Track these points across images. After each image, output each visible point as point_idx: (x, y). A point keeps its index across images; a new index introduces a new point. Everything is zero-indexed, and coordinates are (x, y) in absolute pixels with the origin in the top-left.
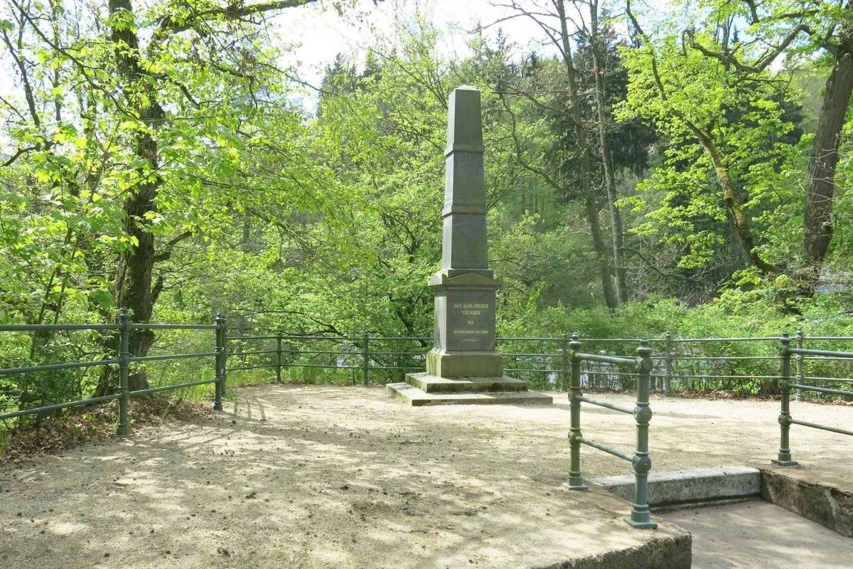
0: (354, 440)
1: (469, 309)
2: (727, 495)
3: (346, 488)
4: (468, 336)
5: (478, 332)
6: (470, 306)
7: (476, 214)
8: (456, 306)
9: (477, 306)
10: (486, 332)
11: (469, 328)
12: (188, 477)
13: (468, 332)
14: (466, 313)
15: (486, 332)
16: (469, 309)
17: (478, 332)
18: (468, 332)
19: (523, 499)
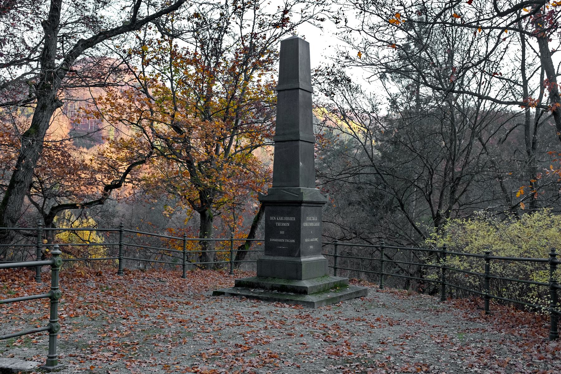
4: (281, 244)
5: (287, 241)
6: (281, 219)
9: (287, 219)
10: (294, 241)
11: (281, 237)
13: (280, 240)
17: (287, 241)
18: (280, 240)
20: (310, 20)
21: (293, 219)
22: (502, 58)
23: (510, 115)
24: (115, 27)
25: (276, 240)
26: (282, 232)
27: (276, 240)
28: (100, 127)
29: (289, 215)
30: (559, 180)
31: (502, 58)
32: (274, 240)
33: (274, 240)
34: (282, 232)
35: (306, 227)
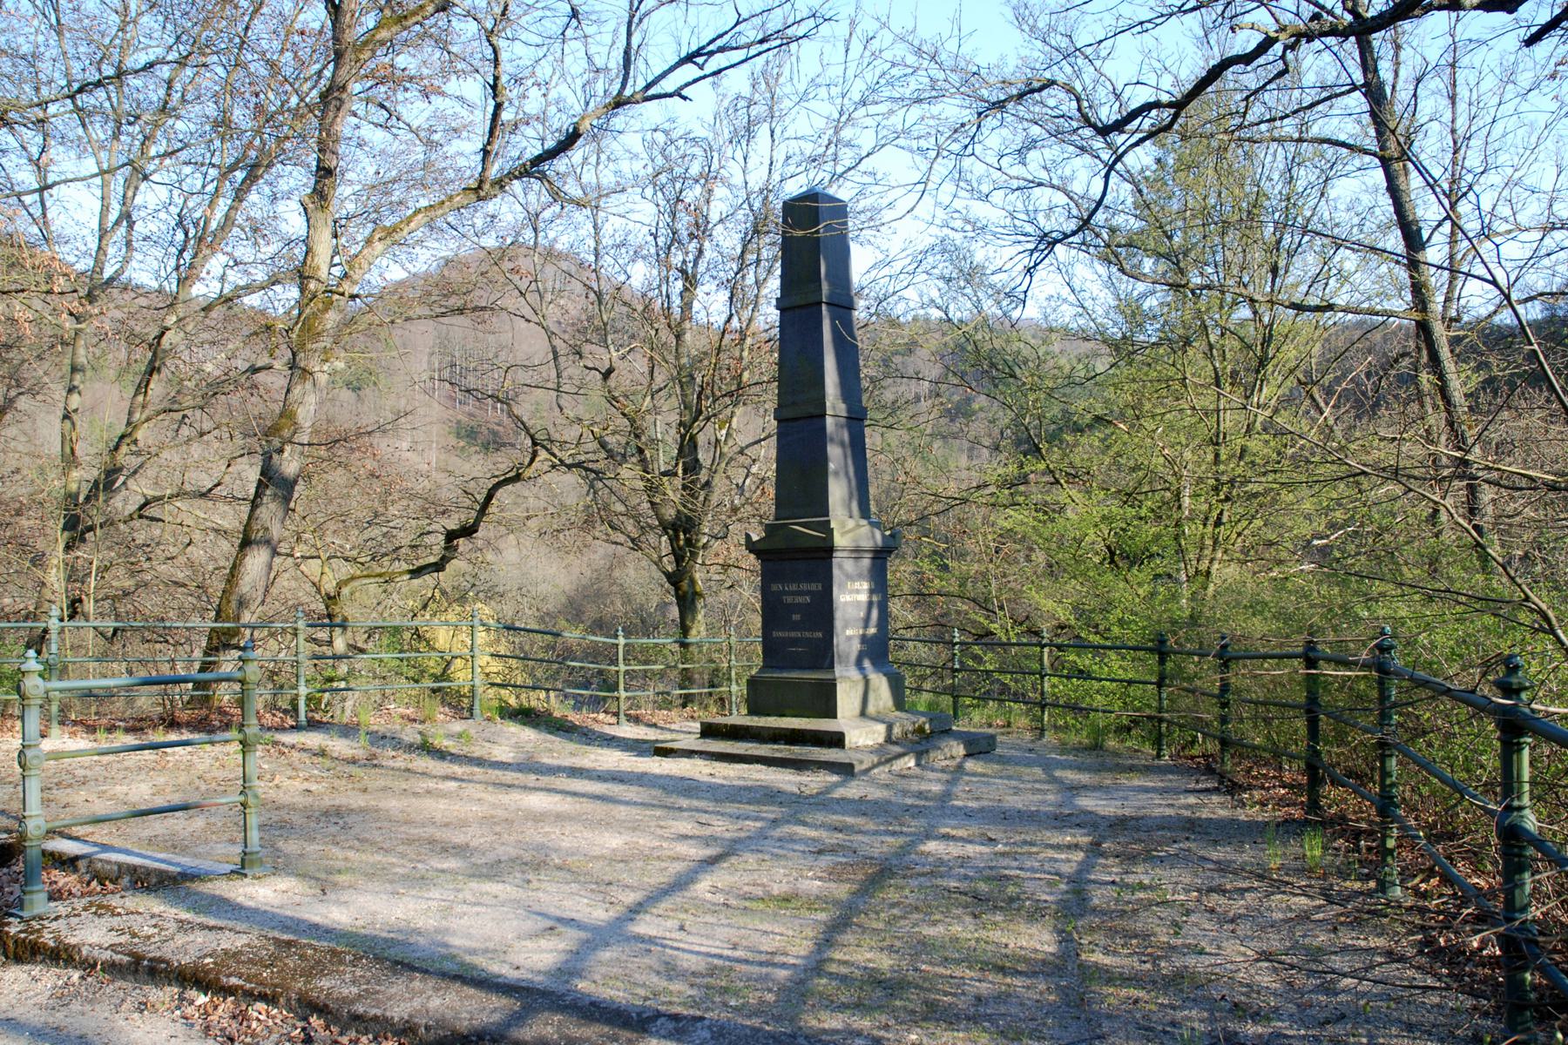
0: (611, 741)
1: (793, 593)
2: (759, 767)
3: (365, 790)
4: (794, 642)
5: (808, 634)
6: (794, 587)
7: (811, 417)
8: (775, 587)
9: (804, 587)
10: (820, 635)
11: (795, 626)
12: (1365, 831)
13: (793, 634)
14: (789, 599)
15: (820, 635)
16: (793, 593)
17: (808, 634)
18: (793, 634)
19: (1432, 185)
20: (901, 142)
21: (816, 587)
22: (247, 28)
23: (826, 861)
24: (861, 363)
25: (786, 634)
26: (796, 617)
27: (786, 634)
28: (24, 668)
29: (809, 578)
30: (316, 17)
31: (247, 28)
32: (780, 634)
33: (780, 634)
34: (796, 617)
35: (846, 603)
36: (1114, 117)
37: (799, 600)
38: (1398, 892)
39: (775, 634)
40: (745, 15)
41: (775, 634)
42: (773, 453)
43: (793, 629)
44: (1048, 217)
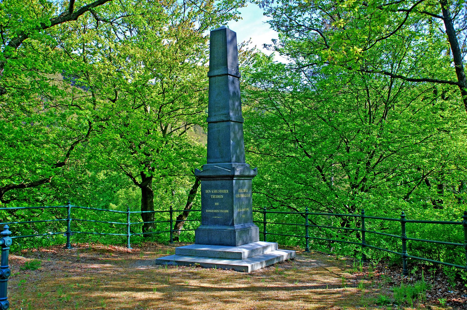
4: (216, 214)
5: (222, 211)
6: (216, 191)
9: (221, 191)
10: (228, 211)
11: (216, 208)
13: (215, 211)
14: (214, 197)
17: (222, 211)
18: (215, 211)
26: (217, 204)
34: (217, 204)
36: (428, 11)
37: (219, 197)
38: (436, 248)
39: (207, 191)
40: (213, 79)
41: (207, 191)
42: (7, 286)
43: (215, 209)
44: (156, 192)
